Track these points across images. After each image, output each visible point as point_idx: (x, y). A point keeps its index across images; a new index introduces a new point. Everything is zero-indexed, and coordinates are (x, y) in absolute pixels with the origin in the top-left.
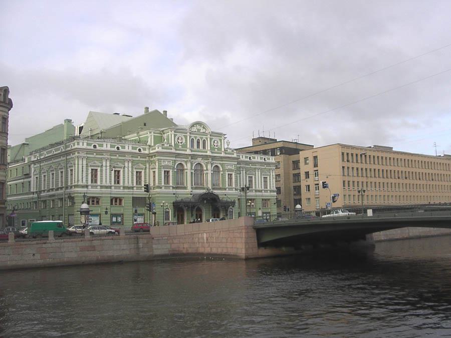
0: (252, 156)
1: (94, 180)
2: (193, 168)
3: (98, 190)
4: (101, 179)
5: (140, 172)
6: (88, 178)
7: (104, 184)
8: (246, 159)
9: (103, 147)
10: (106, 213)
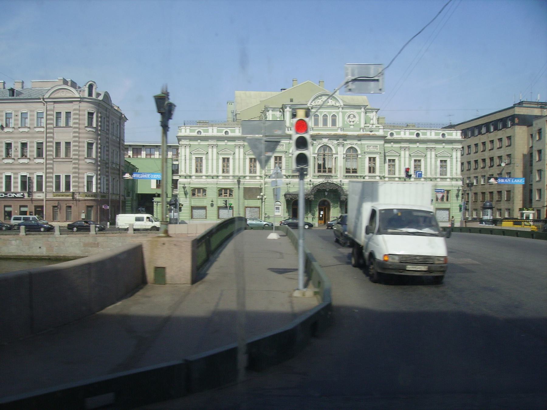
0: (446, 132)
1: (199, 169)
2: (316, 152)
3: (204, 180)
4: (451, 171)
5: (228, 159)
6: (191, 166)
7: (210, 173)
8: (438, 137)
9: (208, 132)
10: (212, 205)
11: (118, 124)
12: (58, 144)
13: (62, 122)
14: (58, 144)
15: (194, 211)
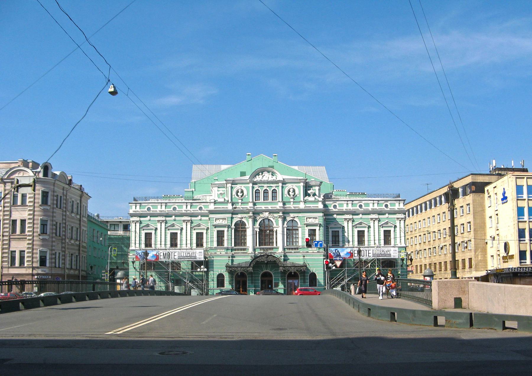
11: (79, 202)
12: (14, 222)
13: (19, 202)
14: (14, 222)
15: (438, 324)
